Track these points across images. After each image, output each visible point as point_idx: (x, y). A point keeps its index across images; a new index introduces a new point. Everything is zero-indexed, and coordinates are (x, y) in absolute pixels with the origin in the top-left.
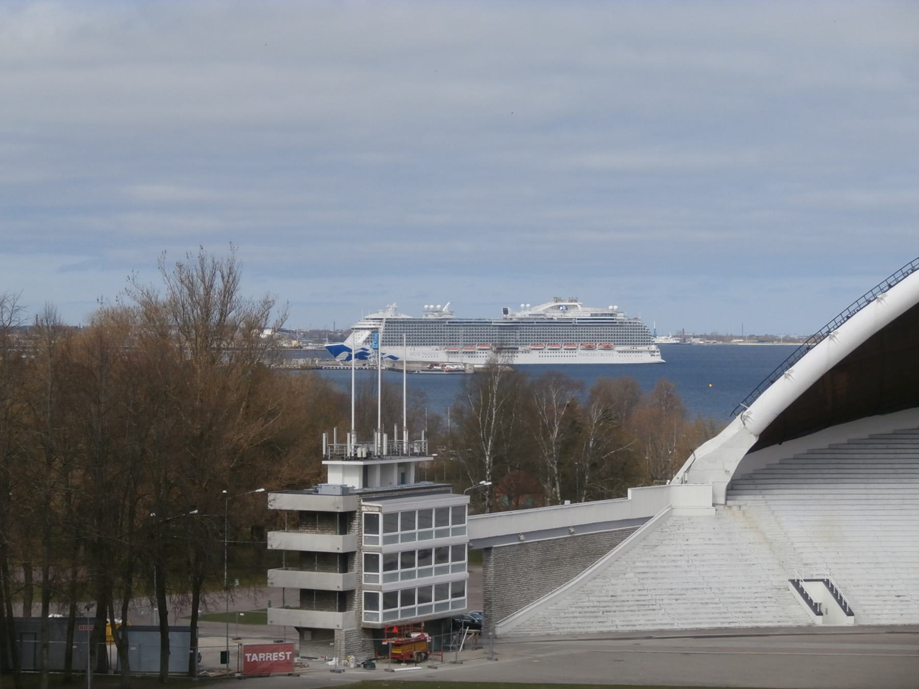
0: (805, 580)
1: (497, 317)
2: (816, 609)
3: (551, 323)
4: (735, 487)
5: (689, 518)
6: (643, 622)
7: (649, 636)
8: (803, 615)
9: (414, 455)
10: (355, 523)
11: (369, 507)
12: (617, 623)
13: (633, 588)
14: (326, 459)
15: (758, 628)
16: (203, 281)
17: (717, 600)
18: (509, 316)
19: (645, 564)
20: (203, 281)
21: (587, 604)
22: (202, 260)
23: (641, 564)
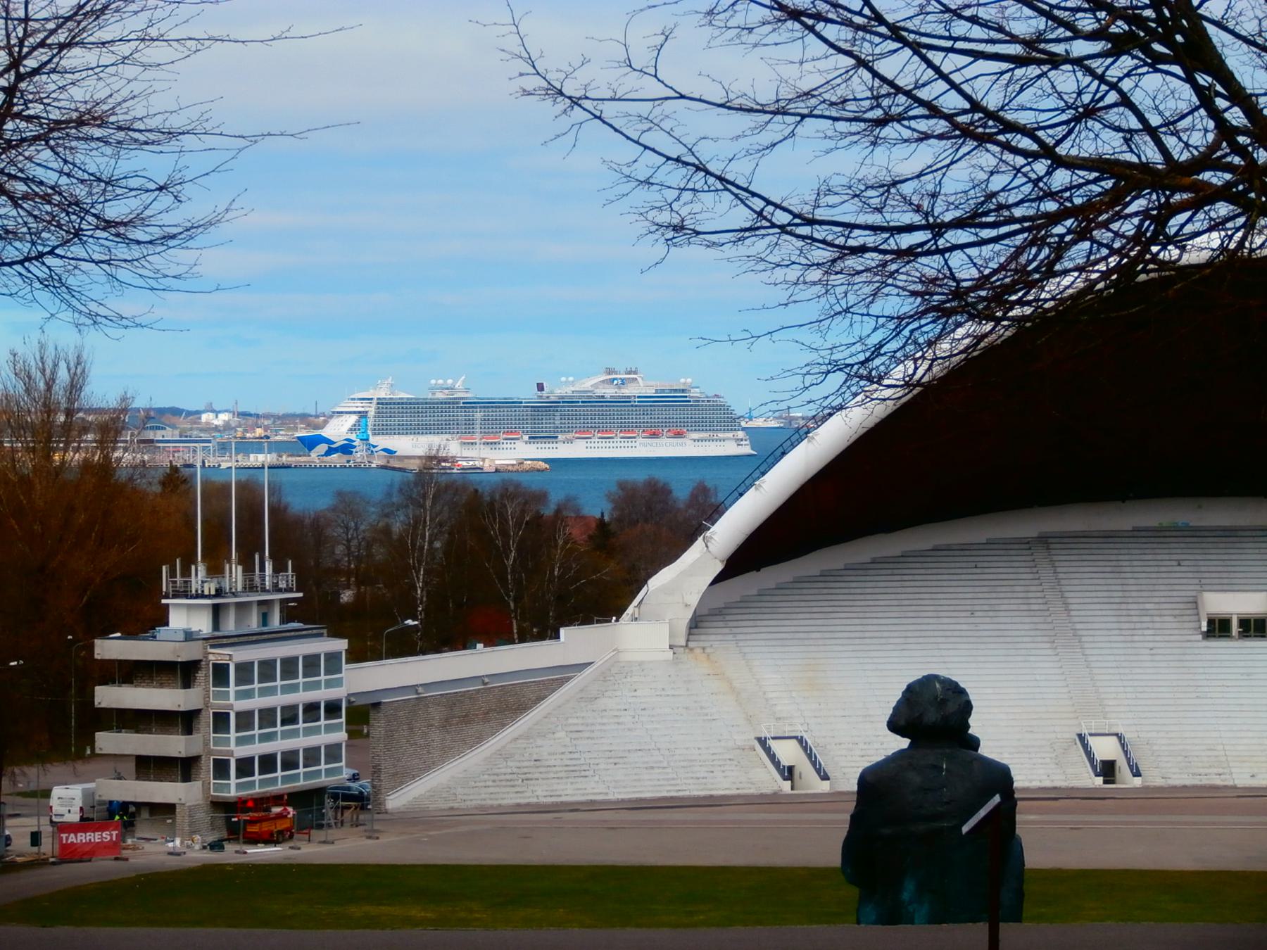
0: (774, 738)
1: (527, 394)
2: (789, 773)
3: (601, 402)
4: (700, 624)
5: (641, 663)
6: (570, 792)
7: (574, 808)
8: (768, 781)
9: (280, 590)
10: (200, 675)
11: (218, 655)
12: (539, 793)
13: (563, 750)
14: (167, 597)
15: (711, 796)
16: (43, 371)
17: (665, 764)
18: (545, 394)
19: (580, 721)
20: (43, 371)
21: (503, 771)
22: (42, 347)
23: (575, 721)
